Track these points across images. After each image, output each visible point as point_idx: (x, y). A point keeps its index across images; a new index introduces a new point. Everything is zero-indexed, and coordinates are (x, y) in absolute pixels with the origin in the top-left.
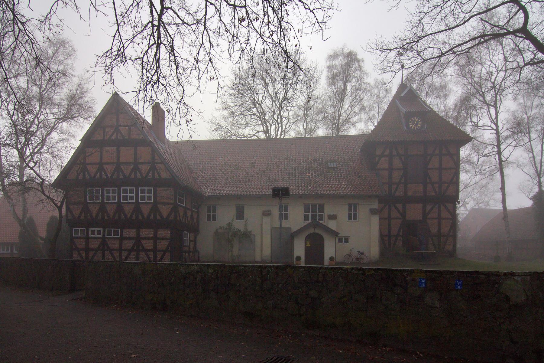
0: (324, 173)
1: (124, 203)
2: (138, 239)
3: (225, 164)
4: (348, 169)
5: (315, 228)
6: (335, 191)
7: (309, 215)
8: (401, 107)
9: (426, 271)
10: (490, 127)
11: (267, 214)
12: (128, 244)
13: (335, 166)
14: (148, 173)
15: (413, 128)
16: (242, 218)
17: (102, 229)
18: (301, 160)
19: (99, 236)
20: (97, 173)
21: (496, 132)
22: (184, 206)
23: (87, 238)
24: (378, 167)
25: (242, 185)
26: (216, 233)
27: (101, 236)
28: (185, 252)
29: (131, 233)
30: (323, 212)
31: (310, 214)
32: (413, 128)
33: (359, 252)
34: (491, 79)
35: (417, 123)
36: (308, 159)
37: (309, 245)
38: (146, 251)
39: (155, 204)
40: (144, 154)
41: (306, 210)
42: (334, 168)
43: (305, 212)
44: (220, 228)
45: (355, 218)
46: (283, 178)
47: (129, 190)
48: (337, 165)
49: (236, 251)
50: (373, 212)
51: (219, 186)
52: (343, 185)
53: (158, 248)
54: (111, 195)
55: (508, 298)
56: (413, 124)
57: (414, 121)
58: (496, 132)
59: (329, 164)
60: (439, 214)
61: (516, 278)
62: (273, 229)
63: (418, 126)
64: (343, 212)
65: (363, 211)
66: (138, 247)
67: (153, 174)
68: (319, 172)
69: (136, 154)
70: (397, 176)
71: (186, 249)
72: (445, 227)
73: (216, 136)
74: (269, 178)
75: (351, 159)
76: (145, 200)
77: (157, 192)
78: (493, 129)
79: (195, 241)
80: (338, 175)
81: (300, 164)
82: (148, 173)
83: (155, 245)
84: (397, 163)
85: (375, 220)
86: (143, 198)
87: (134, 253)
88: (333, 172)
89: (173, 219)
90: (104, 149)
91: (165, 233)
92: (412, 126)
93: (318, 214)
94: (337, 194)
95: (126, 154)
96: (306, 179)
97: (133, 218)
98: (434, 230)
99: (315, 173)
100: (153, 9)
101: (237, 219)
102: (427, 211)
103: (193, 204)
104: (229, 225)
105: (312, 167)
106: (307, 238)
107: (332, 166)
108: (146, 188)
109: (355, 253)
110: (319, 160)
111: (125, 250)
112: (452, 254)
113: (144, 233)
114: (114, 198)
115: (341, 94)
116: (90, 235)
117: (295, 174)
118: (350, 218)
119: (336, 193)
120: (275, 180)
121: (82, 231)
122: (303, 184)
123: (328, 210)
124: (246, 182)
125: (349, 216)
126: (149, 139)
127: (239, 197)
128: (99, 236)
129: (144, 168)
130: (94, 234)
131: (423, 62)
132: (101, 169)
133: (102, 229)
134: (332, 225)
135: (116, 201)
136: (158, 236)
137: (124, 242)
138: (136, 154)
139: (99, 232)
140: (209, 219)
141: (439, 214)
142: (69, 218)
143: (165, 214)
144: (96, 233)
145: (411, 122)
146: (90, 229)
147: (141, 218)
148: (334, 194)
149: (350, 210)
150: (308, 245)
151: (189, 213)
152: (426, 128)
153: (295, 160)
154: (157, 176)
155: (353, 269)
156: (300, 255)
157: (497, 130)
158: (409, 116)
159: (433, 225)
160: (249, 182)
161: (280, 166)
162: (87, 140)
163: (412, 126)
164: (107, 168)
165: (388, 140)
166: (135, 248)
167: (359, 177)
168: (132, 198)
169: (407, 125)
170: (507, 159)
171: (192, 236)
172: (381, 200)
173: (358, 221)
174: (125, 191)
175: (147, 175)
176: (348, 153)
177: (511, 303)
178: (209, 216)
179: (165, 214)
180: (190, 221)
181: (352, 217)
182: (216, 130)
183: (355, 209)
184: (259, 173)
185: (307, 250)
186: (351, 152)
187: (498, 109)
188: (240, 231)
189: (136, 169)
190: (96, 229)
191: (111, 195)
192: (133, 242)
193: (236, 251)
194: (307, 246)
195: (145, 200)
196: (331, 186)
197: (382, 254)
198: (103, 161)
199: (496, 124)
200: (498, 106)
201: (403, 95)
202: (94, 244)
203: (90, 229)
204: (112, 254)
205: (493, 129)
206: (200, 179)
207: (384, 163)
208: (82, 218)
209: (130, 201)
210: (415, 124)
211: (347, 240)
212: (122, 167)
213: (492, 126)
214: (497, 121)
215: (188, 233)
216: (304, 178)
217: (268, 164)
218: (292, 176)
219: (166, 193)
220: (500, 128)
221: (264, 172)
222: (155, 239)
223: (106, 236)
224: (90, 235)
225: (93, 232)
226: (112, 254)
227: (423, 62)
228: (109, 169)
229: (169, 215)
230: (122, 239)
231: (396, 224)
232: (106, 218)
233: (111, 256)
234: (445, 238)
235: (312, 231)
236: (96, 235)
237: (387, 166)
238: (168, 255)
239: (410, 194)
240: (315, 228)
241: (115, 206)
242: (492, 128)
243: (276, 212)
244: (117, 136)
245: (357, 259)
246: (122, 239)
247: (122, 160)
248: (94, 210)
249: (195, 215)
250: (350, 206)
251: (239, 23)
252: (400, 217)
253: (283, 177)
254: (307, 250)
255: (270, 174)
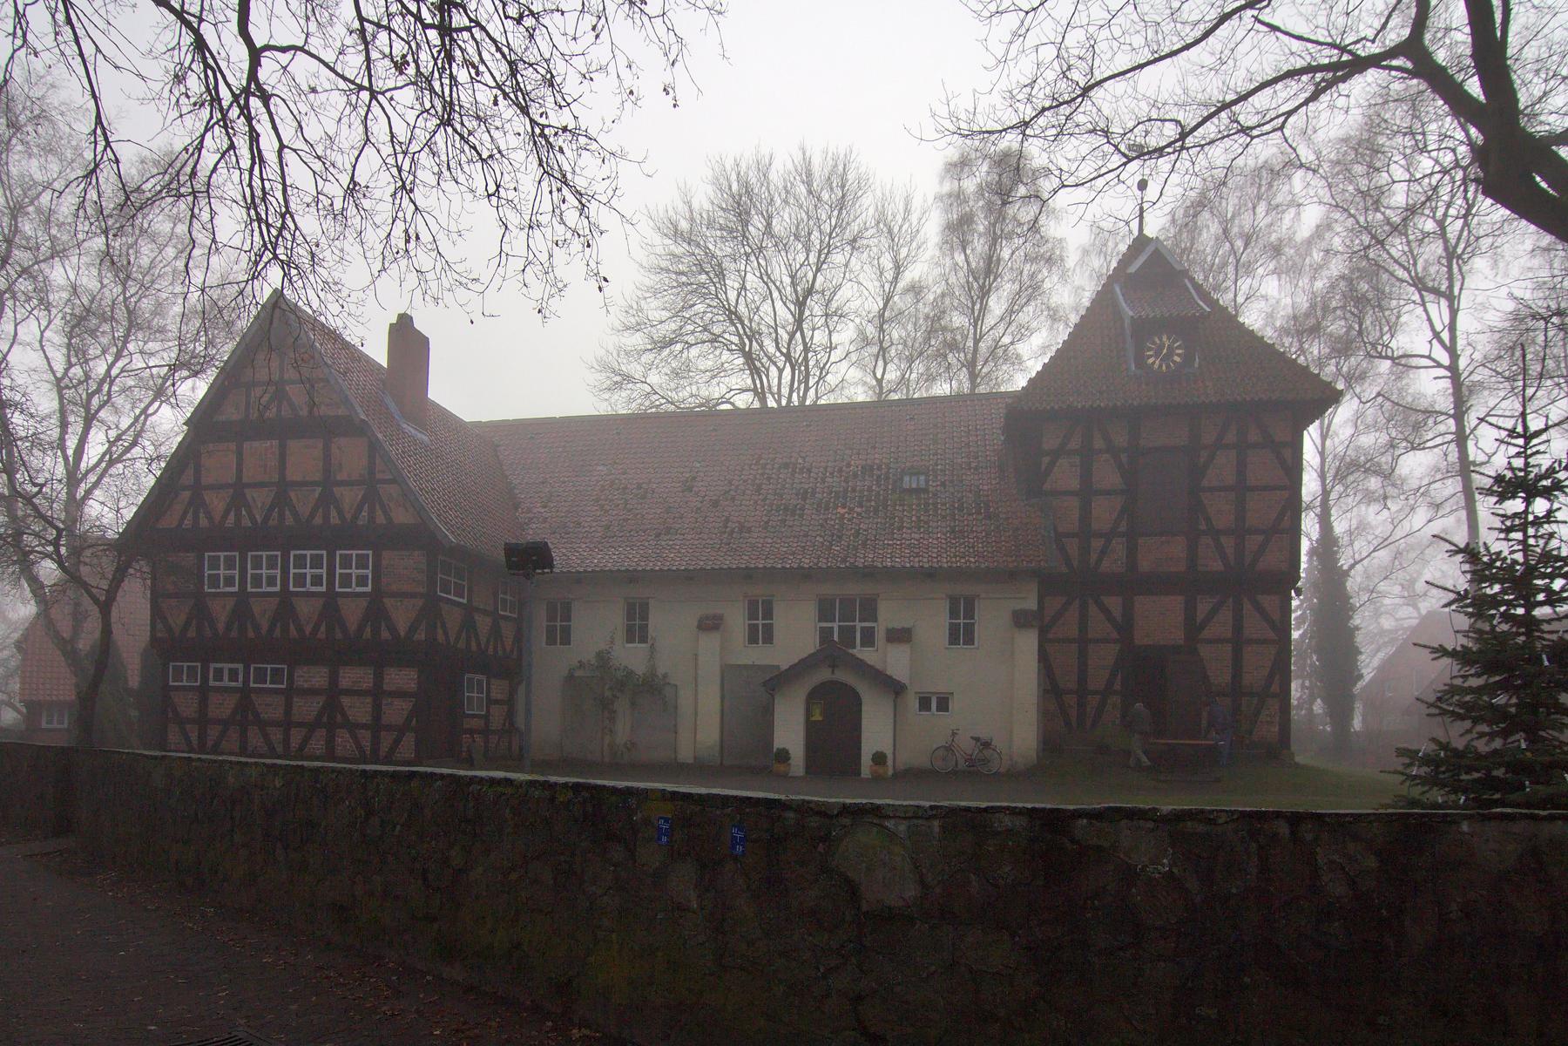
0: (885, 507)
1: (297, 594)
2: (333, 693)
3: (612, 483)
4: (958, 492)
5: (833, 667)
6: (907, 560)
7: (862, 628)
8: (1124, 304)
9: (674, 796)
10: (1429, 357)
11: (710, 624)
12: (307, 709)
13: (922, 484)
14: (359, 509)
15: (1156, 366)
16: (643, 639)
17: (240, 666)
18: (826, 468)
19: (233, 684)
20: (227, 512)
21: (1449, 374)
22: (465, 601)
23: (204, 691)
24: (1047, 487)
25: (647, 544)
26: (570, 678)
27: (239, 684)
28: (471, 732)
29: (316, 676)
30: (876, 621)
31: (836, 625)
32: (1156, 366)
33: (977, 739)
34: (1434, 214)
35: (1171, 352)
36: (849, 465)
37: (820, 719)
38: (353, 727)
39: (377, 596)
40: (350, 457)
41: (825, 612)
42: (918, 491)
43: (820, 620)
44: (581, 665)
45: (970, 640)
46: (767, 523)
47: (311, 559)
48: (927, 481)
49: (623, 730)
50: (1021, 620)
51: (584, 546)
52: (935, 542)
53: (385, 720)
54: (264, 572)
55: (853, 891)
56: (1157, 355)
57: (1161, 347)
58: (1449, 374)
59: (906, 479)
60: (1238, 628)
61: (889, 824)
62: (729, 672)
63: (1174, 362)
64: (932, 622)
65: (992, 618)
66: (331, 717)
67: (282, 515)
68: (873, 503)
69: (327, 457)
70: (1104, 512)
71: (475, 723)
72: (1255, 669)
73: (620, 404)
74: (727, 520)
75: (973, 465)
76: (304, 586)
77: (384, 562)
78: (1439, 365)
79: (510, 702)
80: (926, 511)
81: (823, 481)
82: (359, 509)
83: (377, 715)
84: (1107, 475)
85: (1028, 643)
86: (257, 580)
87: (321, 733)
88: (915, 501)
89: (423, 637)
90: (246, 445)
91: (402, 678)
92: (1154, 362)
93: (859, 625)
94: (912, 567)
95: (304, 459)
96: (832, 523)
97: (318, 636)
98: (1220, 675)
99: (862, 507)
100: (207, 55)
101: (630, 640)
102: (1200, 617)
103: (501, 596)
104: (603, 658)
105: (854, 490)
106: (813, 697)
107: (914, 486)
108: (354, 553)
109: (965, 744)
110: (879, 468)
111: (301, 724)
112: (1277, 750)
113: (350, 676)
114: (271, 581)
115: (986, 275)
116: (211, 683)
117: (802, 509)
118: (954, 638)
119: (908, 565)
120: (742, 528)
121: (192, 673)
122: (821, 540)
123: (890, 615)
124: (658, 535)
125: (972, 633)
126: (357, 414)
127: (632, 577)
128: (233, 684)
129: (349, 497)
130: (221, 680)
131: (1125, 164)
132: (238, 500)
133: (240, 666)
134: (896, 661)
135: (277, 589)
136: (385, 687)
137: (297, 702)
138: (327, 457)
139: (233, 675)
140: (551, 641)
141: (1238, 628)
142: (159, 635)
143: (402, 627)
144: (226, 675)
145: (1150, 349)
146: (213, 666)
147: (339, 636)
148: (904, 567)
149: (954, 613)
150: (817, 717)
151: (483, 623)
152: (1196, 365)
153: (809, 471)
154: (383, 517)
155: (532, 783)
156: (787, 747)
157: (1453, 369)
158: (1144, 330)
159: (1216, 663)
160: (668, 533)
161: (764, 486)
162: (203, 423)
163: (1154, 362)
164: (253, 497)
165: (1075, 404)
166: (325, 719)
167: (988, 517)
168: (317, 580)
169: (1140, 360)
170: (1490, 457)
171: (499, 689)
172: (1048, 584)
173: (978, 649)
174: (300, 562)
175: (355, 517)
176: (968, 445)
177: (865, 907)
178: (551, 632)
179: (402, 627)
180: (488, 641)
181: (961, 635)
182: (618, 386)
183: (970, 613)
184: (699, 509)
185: (813, 733)
186: (977, 442)
187: (1456, 303)
188: (630, 673)
189: (327, 500)
190: (226, 666)
191: (264, 572)
192: (316, 704)
193: (623, 730)
194: (813, 719)
195: (304, 586)
196: (901, 544)
197: (1050, 744)
198: (245, 480)
199: (1452, 351)
200: (1456, 292)
201: (1132, 269)
202: (222, 707)
203: (213, 666)
204: (266, 736)
205: (1439, 365)
206: (534, 526)
207: (1065, 475)
208: (192, 633)
209: (314, 589)
210: (1163, 355)
211: (943, 704)
212: (292, 495)
213: (1433, 356)
214: (1453, 338)
215: (483, 678)
216: (826, 520)
217: (730, 483)
218: (793, 514)
219: (406, 566)
220: (1462, 363)
221: (715, 504)
222: (377, 694)
223: (252, 685)
224: (211, 683)
225: (219, 674)
226: (266, 736)
227: (1125, 164)
228: (260, 499)
229: (413, 629)
230: (290, 693)
231: (1103, 658)
232: (251, 634)
233: (262, 740)
234: (1255, 700)
235: (824, 675)
236: (226, 682)
237: (1075, 484)
238: (409, 740)
239: (1145, 565)
240: (833, 667)
241: (364, 603)
242: (1434, 360)
243: (737, 620)
244: (279, 411)
245: (971, 761)
246: (290, 693)
247: (293, 475)
248: (221, 612)
249: (508, 631)
250: (954, 602)
251: (472, 78)
252: (1115, 635)
253: (765, 519)
254: (811, 728)
255: (730, 509)
